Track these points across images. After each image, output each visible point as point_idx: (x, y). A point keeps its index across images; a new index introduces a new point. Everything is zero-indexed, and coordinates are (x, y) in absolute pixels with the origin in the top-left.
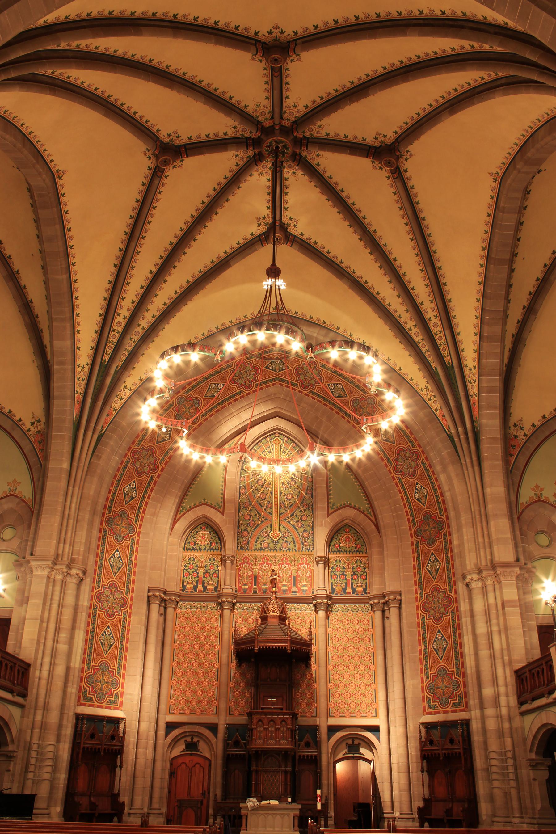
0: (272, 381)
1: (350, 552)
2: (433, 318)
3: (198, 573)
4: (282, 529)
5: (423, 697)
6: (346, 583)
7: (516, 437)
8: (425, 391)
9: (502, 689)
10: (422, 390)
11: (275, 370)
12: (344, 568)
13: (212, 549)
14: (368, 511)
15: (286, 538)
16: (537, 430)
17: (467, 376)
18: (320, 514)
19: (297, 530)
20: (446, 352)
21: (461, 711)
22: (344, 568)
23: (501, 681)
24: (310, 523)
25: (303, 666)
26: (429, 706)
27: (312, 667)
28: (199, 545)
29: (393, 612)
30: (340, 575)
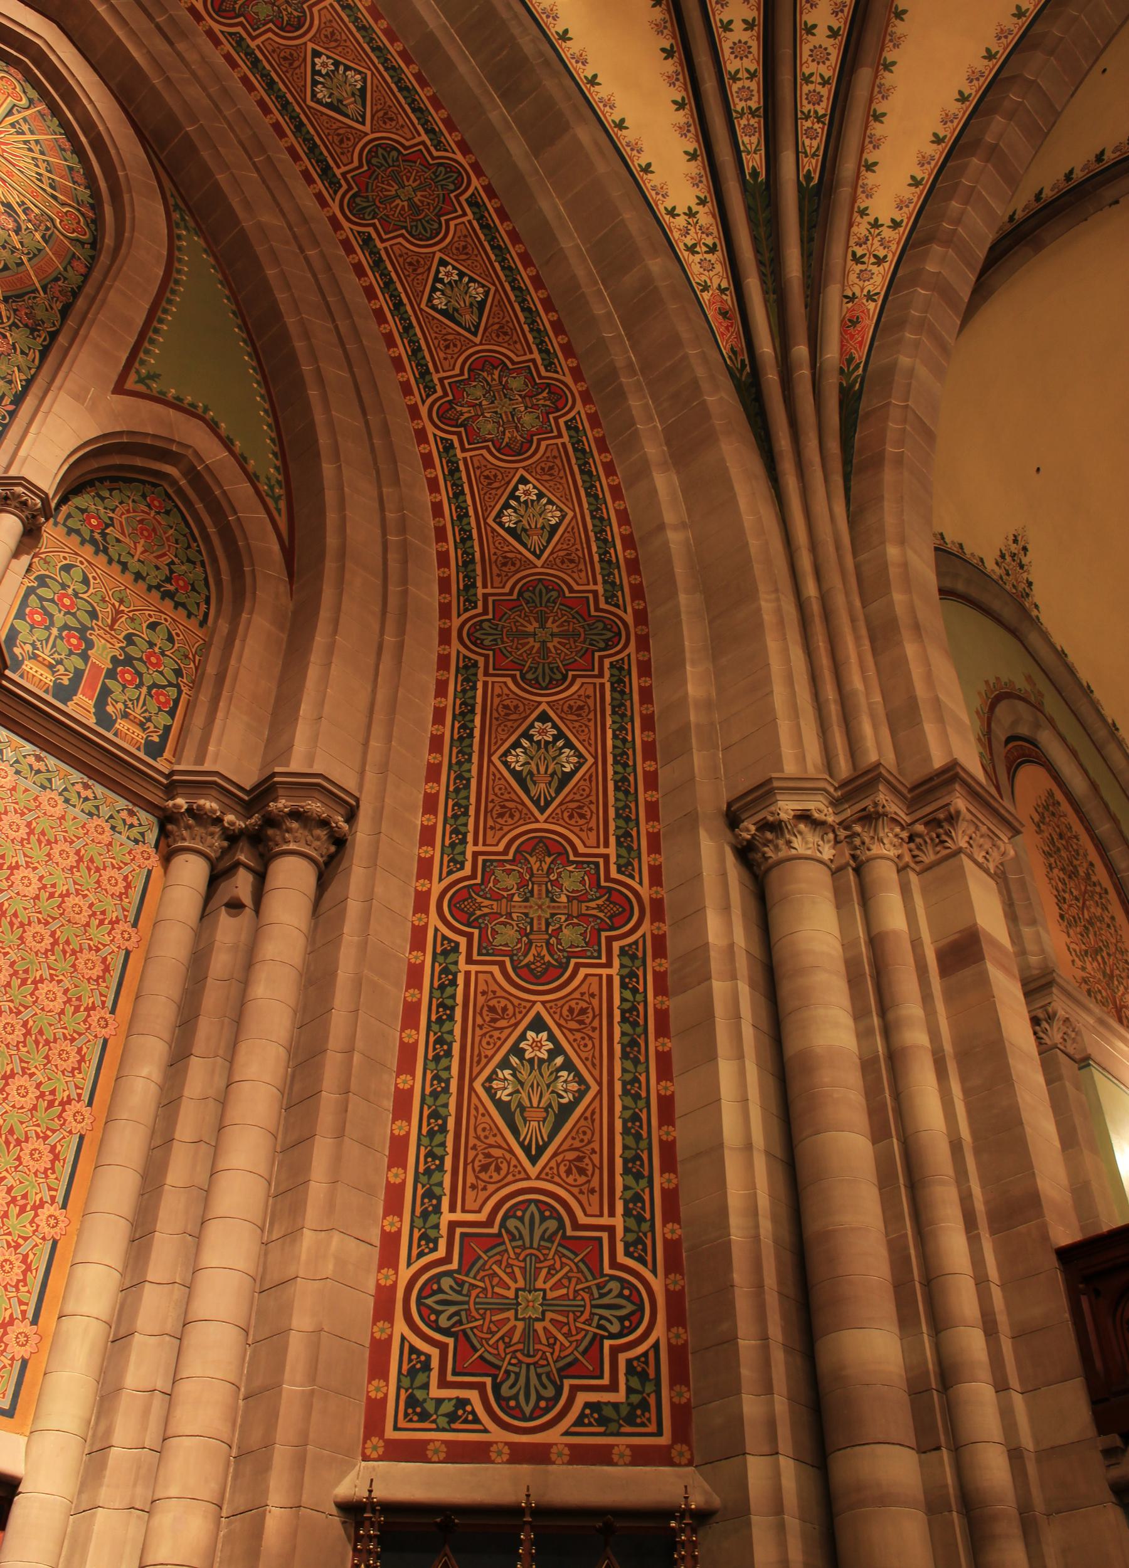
1: (138, 576)
2: (821, 32)
5: (380, 1349)
6: (78, 674)
8: (681, 221)
9: (972, 1343)
12: (93, 615)
14: (272, 488)
20: (815, 143)
21: (641, 1457)
22: (93, 615)
23: (964, 1299)
24: (19, 379)
26: (412, 1402)
29: (293, 876)
30: (66, 627)
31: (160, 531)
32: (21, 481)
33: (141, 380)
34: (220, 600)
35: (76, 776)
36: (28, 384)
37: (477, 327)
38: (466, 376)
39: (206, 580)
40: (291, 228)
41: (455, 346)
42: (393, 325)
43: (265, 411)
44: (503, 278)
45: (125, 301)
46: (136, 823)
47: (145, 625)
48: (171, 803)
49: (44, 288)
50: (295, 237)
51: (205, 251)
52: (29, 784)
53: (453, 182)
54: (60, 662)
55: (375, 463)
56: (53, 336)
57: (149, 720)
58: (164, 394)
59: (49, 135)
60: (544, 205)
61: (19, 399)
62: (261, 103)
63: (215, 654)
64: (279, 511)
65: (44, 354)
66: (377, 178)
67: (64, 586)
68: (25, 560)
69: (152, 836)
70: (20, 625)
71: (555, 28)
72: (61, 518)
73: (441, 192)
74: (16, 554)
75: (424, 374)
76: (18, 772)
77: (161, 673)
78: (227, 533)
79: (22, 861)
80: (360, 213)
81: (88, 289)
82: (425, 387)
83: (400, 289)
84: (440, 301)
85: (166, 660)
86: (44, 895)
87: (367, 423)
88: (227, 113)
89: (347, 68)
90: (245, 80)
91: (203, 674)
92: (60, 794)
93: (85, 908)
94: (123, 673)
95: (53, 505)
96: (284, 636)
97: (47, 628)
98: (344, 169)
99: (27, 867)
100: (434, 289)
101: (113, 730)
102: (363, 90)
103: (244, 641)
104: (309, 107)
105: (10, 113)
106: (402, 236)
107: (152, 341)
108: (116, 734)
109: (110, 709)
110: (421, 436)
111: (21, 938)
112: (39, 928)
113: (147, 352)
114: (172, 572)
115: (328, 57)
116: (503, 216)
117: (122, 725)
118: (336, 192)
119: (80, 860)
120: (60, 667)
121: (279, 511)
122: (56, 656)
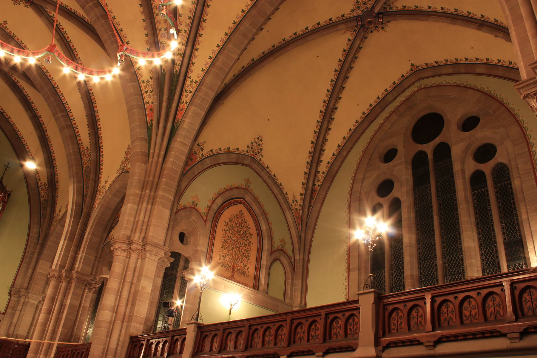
7: (196, 153)
8: (145, 84)
10: (143, 82)
16: (213, 155)
17: (187, 85)
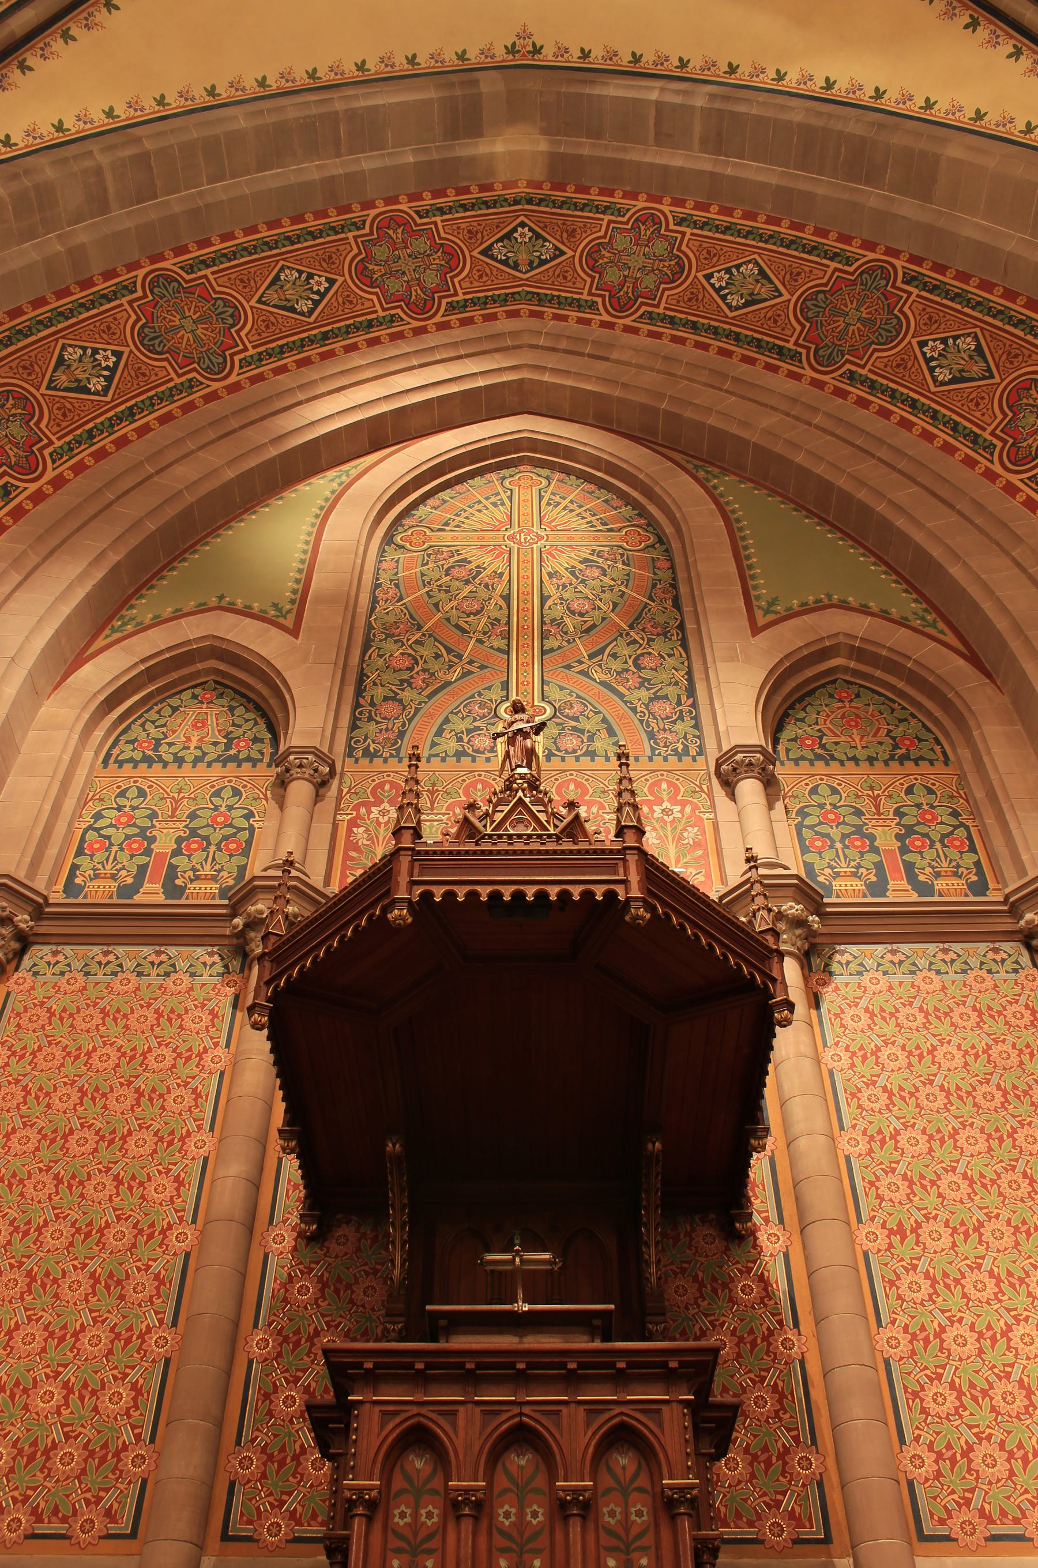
0: (505, 300)
3: (153, 840)
4: (554, 694)
6: (879, 866)
11: (516, 267)
12: (858, 813)
13: (234, 759)
14: (923, 619)
15: (576, 719)
18: (721, 630)
19: (621, 696)
22: (858, 813)
24: (680, 675)
25: (705, 1236)
27: (762, 1237)
28: (173, 749)
30: (844, 836)
31: (862, 715)
32: (736, 749)
33: (767, 612)
34: (947, 735)
35: (932, 948)
36: (690, 673)
37: (989, 370)
38: (1010, 415)
39: (924, 726)
40: (788, 415)
41: (983, 398)
42: (921, 423)
43: (874, 564)
44: (979, 316)
45: (712, 562)
46: (1005, 956)
47: (903, 794)
48: (1022, 923)
49: (651, 598)
50: (797, 418)
51: (741, 482)
52: (900, 977)
53: (881, 278)
54: (858, 866)
55: (990, 538)
56: (681, 627)
57: (958, 866)
58: (791, 608)
59: (575, 490)
60: (968, 232)
61: (691, 691)
62: (698, 345)
63: (973, 779)
64: (942, 632)
65: (684, 645)
66: (822, 325)
67: (821, 806)
68: (779, 806)
69: (1025, 959)
70: (811, 858)
71: (865, 96)
72: (782, 756)
73: (878, 294)
74: (770, 807)
75: (975, 439)
76: (885, 973)
77: (942, 823)
78: (914, 678)
79: (879, 1042)
80: (830, 361)
81: (681, 575)
82: (984, 449)
83: (906, 391)
84: (943, 375)
85: (938, 811)
86: (970, 1059)
87: (959, 513)
88: (680, 373)
89: (738, 267)
90: (674, 339)
91: (975, 801)
92: (930, 970)
93: (1010, 1050)
94: (912, 843)
95: (770, 750)
96: (1019, 727)
97: (831, 847)
98: (793, 340)
99: (942, 1044)
100: (932, 370)
101: (936, 894)
102: (762, 272)
103: (989, 753)
104: (733, 318)
105: (541, 498)
106: (875, 350)
107: (753, 577)
108: (940, 895)
109: (922, 878)
110: (1011, 490)
111: (975, 1105)
112: (984, 1088)
113: (755, 588)
114: (894, 739)
115: (719, 271)
116: (941, 269)
117: (939, 884)
118: (800, 361)
119: (980, 1014)
120: (861, 870)
121: (942, 632)
122: (853, 864)
